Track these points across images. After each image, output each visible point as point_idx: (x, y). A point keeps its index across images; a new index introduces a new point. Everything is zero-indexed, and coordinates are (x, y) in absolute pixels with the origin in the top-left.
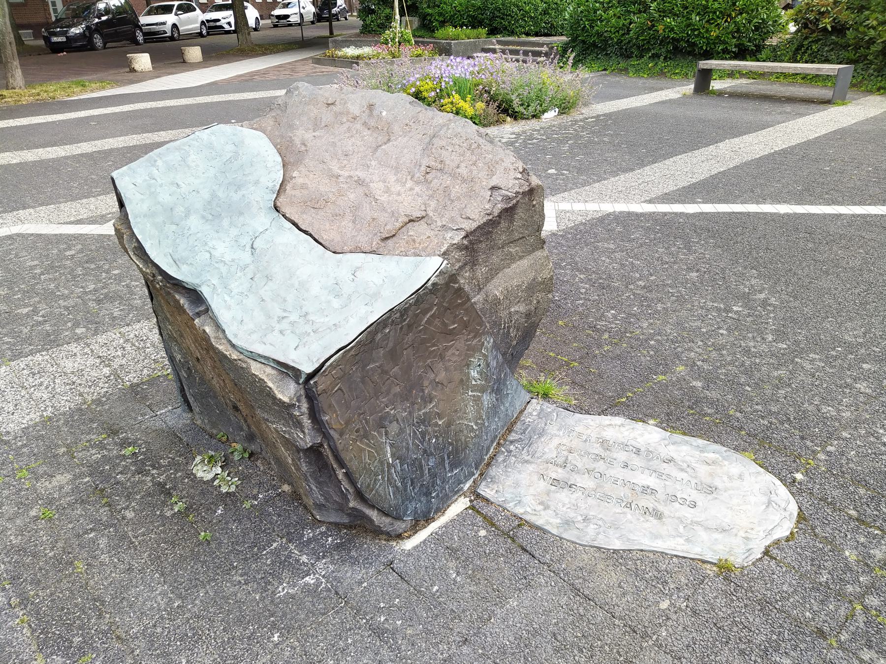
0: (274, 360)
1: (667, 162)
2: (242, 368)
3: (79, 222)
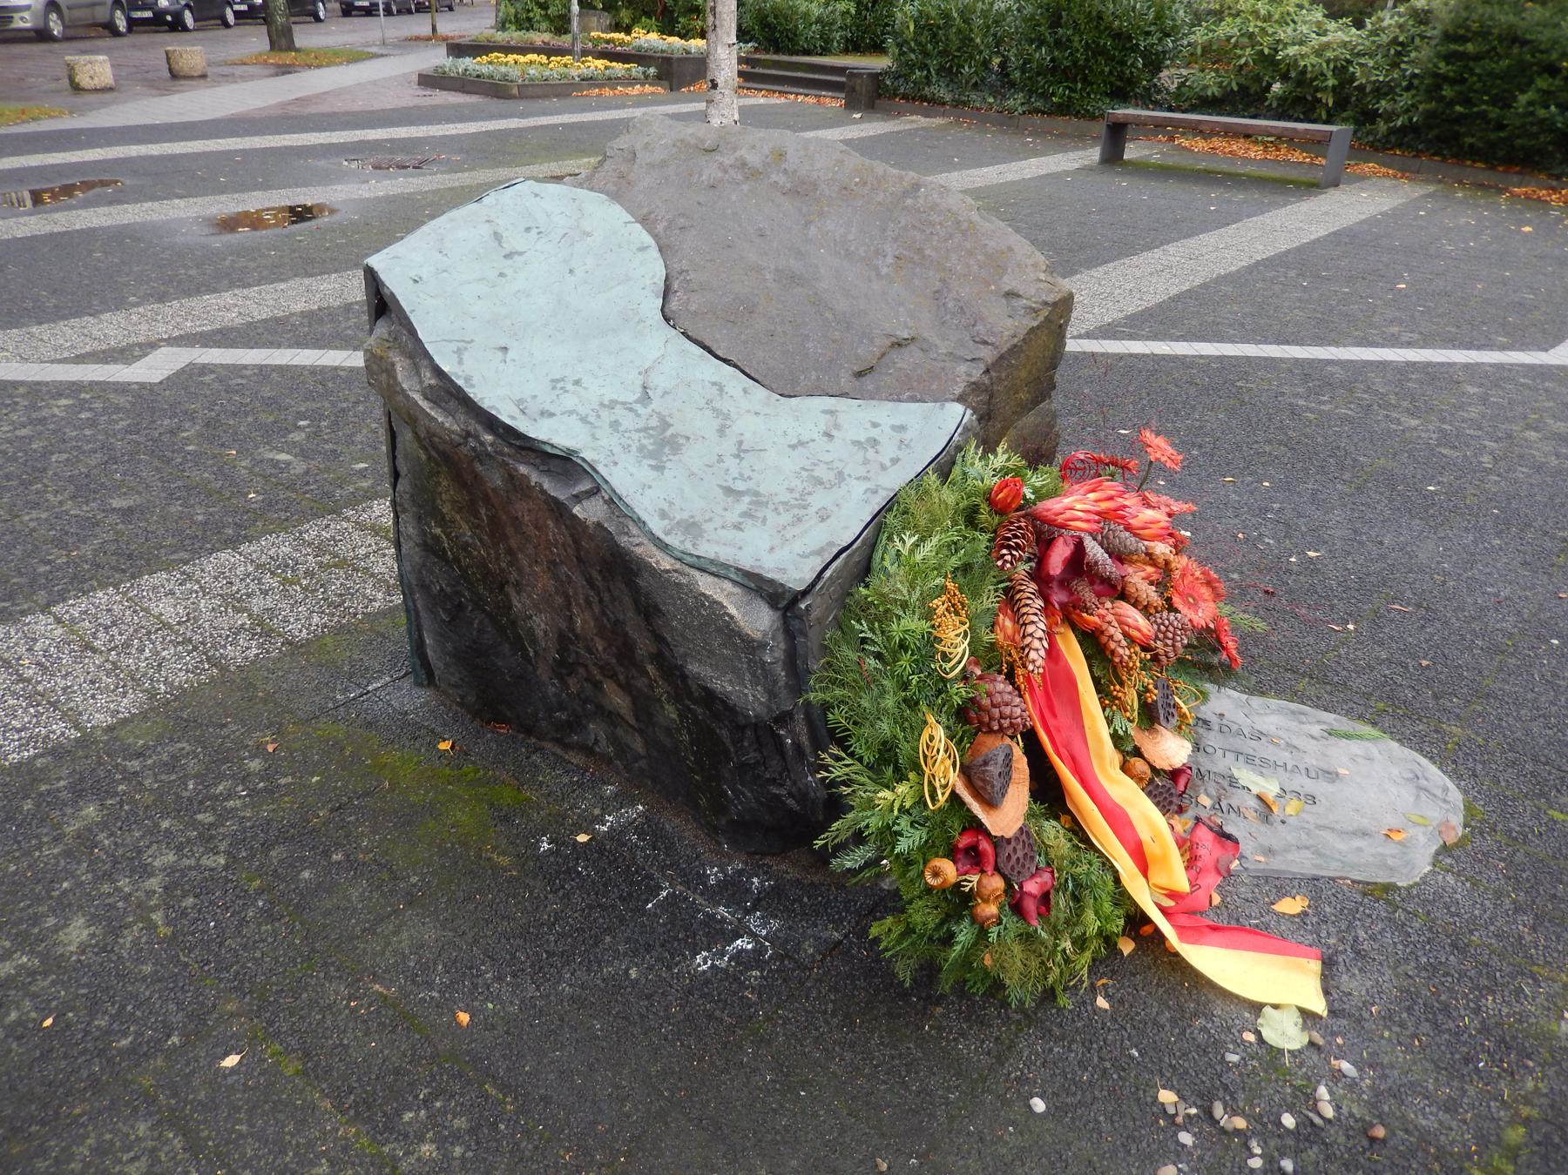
0: (737, 569)
1: (1093, 272)
2: (678, 585)
3: (80, 359)
